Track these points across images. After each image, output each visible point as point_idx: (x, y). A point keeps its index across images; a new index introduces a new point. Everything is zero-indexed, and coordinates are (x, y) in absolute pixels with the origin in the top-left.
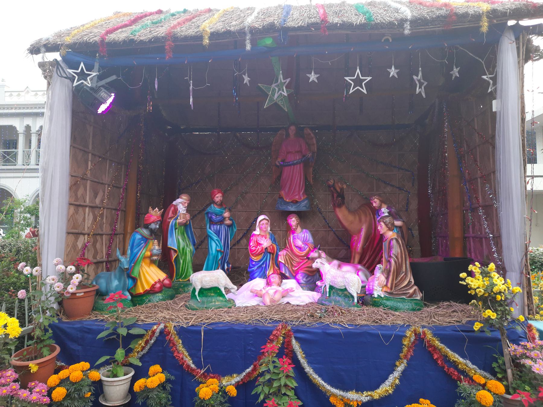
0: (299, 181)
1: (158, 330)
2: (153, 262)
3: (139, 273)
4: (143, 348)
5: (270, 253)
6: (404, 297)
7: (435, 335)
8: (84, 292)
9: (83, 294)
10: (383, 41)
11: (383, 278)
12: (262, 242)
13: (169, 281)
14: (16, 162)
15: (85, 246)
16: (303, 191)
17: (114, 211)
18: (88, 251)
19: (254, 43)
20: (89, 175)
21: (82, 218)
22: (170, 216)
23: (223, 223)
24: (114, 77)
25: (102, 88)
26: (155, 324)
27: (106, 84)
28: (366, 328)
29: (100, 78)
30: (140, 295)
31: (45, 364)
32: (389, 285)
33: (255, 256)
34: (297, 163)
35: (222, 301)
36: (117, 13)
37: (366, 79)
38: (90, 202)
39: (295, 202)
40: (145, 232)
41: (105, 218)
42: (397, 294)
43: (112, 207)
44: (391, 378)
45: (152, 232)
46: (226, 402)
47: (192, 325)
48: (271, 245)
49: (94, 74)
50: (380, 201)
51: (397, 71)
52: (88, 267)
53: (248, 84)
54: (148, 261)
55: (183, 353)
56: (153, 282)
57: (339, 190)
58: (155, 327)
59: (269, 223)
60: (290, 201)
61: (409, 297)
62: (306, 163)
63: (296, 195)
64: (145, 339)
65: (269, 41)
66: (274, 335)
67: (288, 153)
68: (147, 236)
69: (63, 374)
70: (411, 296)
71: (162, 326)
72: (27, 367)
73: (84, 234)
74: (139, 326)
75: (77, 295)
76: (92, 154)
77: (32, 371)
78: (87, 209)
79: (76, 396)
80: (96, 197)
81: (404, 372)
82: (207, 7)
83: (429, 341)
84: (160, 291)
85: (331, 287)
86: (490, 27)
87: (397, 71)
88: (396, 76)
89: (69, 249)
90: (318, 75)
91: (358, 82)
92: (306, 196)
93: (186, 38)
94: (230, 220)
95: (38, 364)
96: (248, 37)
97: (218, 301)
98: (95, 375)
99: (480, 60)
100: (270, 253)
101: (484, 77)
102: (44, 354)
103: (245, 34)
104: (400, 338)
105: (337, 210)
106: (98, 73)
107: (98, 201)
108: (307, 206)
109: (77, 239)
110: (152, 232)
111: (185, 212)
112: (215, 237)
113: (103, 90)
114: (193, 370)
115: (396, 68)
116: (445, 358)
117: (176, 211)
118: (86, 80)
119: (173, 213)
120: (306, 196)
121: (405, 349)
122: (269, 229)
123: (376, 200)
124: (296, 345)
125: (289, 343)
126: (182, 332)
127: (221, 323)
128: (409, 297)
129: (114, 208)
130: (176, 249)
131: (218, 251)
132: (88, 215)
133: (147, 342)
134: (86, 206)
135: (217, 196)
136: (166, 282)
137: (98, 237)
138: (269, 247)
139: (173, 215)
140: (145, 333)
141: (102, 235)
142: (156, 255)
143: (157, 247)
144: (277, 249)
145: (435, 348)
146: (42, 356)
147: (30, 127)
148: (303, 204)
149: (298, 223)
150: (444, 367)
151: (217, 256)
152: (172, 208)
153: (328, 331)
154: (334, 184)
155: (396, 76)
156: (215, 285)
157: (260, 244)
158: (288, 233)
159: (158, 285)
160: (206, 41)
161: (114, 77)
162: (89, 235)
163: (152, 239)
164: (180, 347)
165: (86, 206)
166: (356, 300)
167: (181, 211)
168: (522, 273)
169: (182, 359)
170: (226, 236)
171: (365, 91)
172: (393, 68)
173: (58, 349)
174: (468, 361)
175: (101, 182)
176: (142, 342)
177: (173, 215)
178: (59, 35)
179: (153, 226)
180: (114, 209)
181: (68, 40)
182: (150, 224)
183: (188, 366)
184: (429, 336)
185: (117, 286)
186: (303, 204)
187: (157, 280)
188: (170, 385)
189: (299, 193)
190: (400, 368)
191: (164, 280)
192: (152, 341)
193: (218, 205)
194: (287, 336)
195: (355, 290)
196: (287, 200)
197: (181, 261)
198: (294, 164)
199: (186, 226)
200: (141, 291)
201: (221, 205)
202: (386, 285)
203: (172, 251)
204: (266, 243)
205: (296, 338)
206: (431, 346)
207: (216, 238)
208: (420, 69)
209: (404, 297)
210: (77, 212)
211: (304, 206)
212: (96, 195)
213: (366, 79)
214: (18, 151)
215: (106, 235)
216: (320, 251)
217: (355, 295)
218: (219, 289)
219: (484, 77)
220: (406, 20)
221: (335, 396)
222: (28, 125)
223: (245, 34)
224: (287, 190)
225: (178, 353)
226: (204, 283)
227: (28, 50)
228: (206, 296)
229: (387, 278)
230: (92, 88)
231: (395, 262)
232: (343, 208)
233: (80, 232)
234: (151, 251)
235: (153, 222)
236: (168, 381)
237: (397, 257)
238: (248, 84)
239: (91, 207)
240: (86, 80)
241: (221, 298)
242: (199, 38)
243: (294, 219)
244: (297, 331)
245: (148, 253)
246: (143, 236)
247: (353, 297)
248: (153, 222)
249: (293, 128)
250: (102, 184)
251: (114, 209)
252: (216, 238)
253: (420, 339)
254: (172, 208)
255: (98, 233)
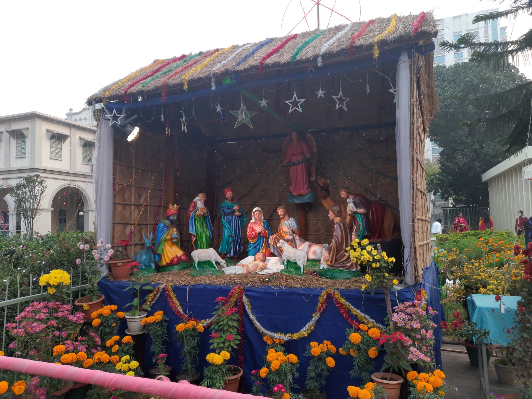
0: (302, 177)
1: (162, 288)
2: (174, 243)
3: (163, 251)
4: (153, 299)
5: (263, 237)
6: (341, 269)
7: (342, 295)
8: (123, 263)
9: (121, 264)
10: (308, 71)
13: (186, 257)
15: (132, 232)
16: (306, 186)
17: (156, 208)
18: (135, 236)
19: (217, 83)
20: (133, 183)
21: (129, 213)
22: (191, 210)
23: (234, 215)
24: (136, 116)
25: (128, 125)
26: (160, 284)
27: (133, 120)
28: (295, 289)
29: (127, 117)
30: (164, 267)
31: (94, 306)
33: (251, 239)
34: (299, 164)
35: (214, 271)
36: (156, 61)
37: (301, 101)
38: (134, 202)
39: (301, 195)
40: (168, 222)
41: (148, 213)
42: (337, 267)
43: (154, 204)
44: (307, 326)
45: (172, 222)
46: (197, 336)
47: (183, 285)
48: (264, 230)
49: (122, 116)
50: (347, 192)
51: (324, 92)
52: (135, 247)
53: (221, 112)
54: (170, 243)
55: (176, 304)
56: (171, 257)
57: (322, 185)
58: (160, 286)
59: (262, 214)
60: (297, 195)
61: (346, 269)
62: (308, 163)
63: (301, 190)
64: (153, 294)
65: (228, 81)
66: (232, 293)
67: (293, 154)
68: (168, 225)
69: (100, 311)
70: (348, 268)
71: (164, 285)
72: (82, 306)
73: (131, 224)
74: (151, 285)
75: (118, 264)
76: (135, 168)
77: (85, 309)
78: (133, 207)
79: (106, 325)
80: (140, 198)
81: (318, 322)
82: (216, 48)
83: (336, 300)
84: (178, 263)
85: (288, 261)
86: (380, 54)
87: (324, 92)
88: (323, 96)
89: (119, 235)
90: (267, 101)
91: (295, 104)
92: (309, 190)
93: (174, 86)
94: (239, 212)
95: (89, 305)
96: (213, 80)
97: (211, 271)
98: (121, 314)
99: (386, 76)
100: (263, 237)
101: (391, 91)
102: (94, 300)
103: (211, 78)
104: (316, 297)
105: (84, 210)
106: (125, 115)
107: (142, 201)
108: (311, 198)
109: (125, 228)
110: (172, 222)
111: (203, 207)
112: (227, 225)
113: (129, 125)
114: (181, 315)
116: (349, 311)
117: (195, 206)
118: (117, 121)
119: (193, 208)
120: (309, 190)
121: (320, 305)
122: (263, 218)
123: (343, 192)
124: (245, 300)
125: (241, 298)
126: (176, 289)
127: (202, 284)
128: (346, 269)
129: (157, 205)
130: (195, 234)
132: (134, 211)
133: (155, 296)
134: (132, 205)
135: (228, 193)
136: (183, 258)
137: (144, 227)
138: (262, 232)
139: (193, 209)
140: (153, 289)
141: (146, 225)
142: (174, 238)
143: (175, 233)
144: (269, 234)
145: (342, 305)
146: (92, 300)
148: (307, 197)
149: (286, 213)
150: (348, 319)
151: (229, 240)
152: (193, 204)
153: (267, 291)
154: (316, 180)
155: (323, 96)
156: (209, 259)
157: (253, 230)
159: (176, 260)
160: (186, 87)
161: (136, 116)
162: (134, 224)
163: (172, 227)
164: (174, 300)
165: (132, 205)
167: (199, 206)
168: (411, 247)
169: (175, 307)
170: (237, 224)
172: (320, 91)
173: (103, 297)
174: (367, 316)
175: (144, 187)
176: (152, 295)
177: (193, 209)
178: (104, 90)
179: (172, 218)
180: (157, 206)
181: (108, 94)
182: (170, 216)
183: (178, 312)
184: (337, 295)
185: (145, 259)
186: (307, 197)
187: (175, 255)
188: (166, 324)
189: (303, 188)
190: (315, 317)
191: (181, 256)
192: (158, 295)
193: (230, 201)
194: (241, 293)
196: (295, 194)
197: (199, 244)
198: (297, 164)
199: (204, 217)
200: (165, 264)
201: (232, 200)
203: (192, 236)
204: (258, 229)
205: (247, 296)
206: (339, 303)
207: (227, 226)
208: (341, 89)
209: (341, 269)
210: (124, 209)
211: (308, 199)
212: (140, 197)
213: (301, 101)
215: (150, 225)
216: (294, 235)
217: (302, 267)
218: (212, 263)
219: (391, 91)
220: (319, 56)
221: (266, 335)
223: (211, 78)
224: (293, 186)
225: (173, 303)
226: (200, 258)
227: (87, 103)
228: (203, 267)
230: (121, 126)
231: (336, 242)
232: (328, 199)
233: (127, 222)
234: (171, 235)
235: (171, 215)
236: (163, 321)
237: (337, 238)
238: (221, 112)
239: (135, 205)
240: (117, 121)
241: (213, 269)
242: (181, 84)
243: (281, 210)
244: (248, 290)
245: (169, 237)
246: (165, 225)
248: (171, 215)
249: (294, 134)
250: (145, 188)
251: (157, 206)
252: (227, 226)
253: (330, 297)
254: (193, 204)
255: (142, 223)
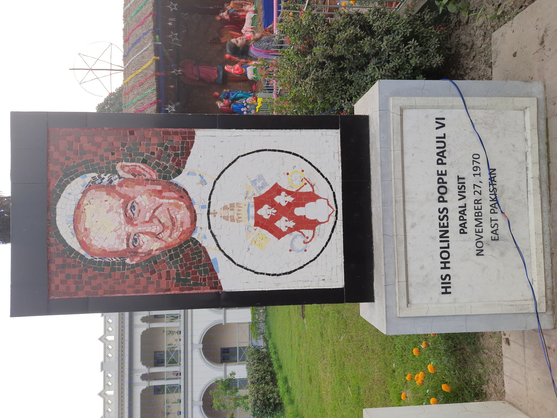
11: (248, 6)
12: (237, 68)
14: (176, 387)
32: (250, 3)
115: (169, 23)
131: (242, 93)
147: (143, 317)
158: (234, 26)
166: (256, 14)
171: (176, 9)
195: (253, 15)
202: (250, 4)
214: (167, 385)
217: (254, 14)
218: (254, 69)
222: (141, 320)
229: (248, 4)
247: (255, 15)
